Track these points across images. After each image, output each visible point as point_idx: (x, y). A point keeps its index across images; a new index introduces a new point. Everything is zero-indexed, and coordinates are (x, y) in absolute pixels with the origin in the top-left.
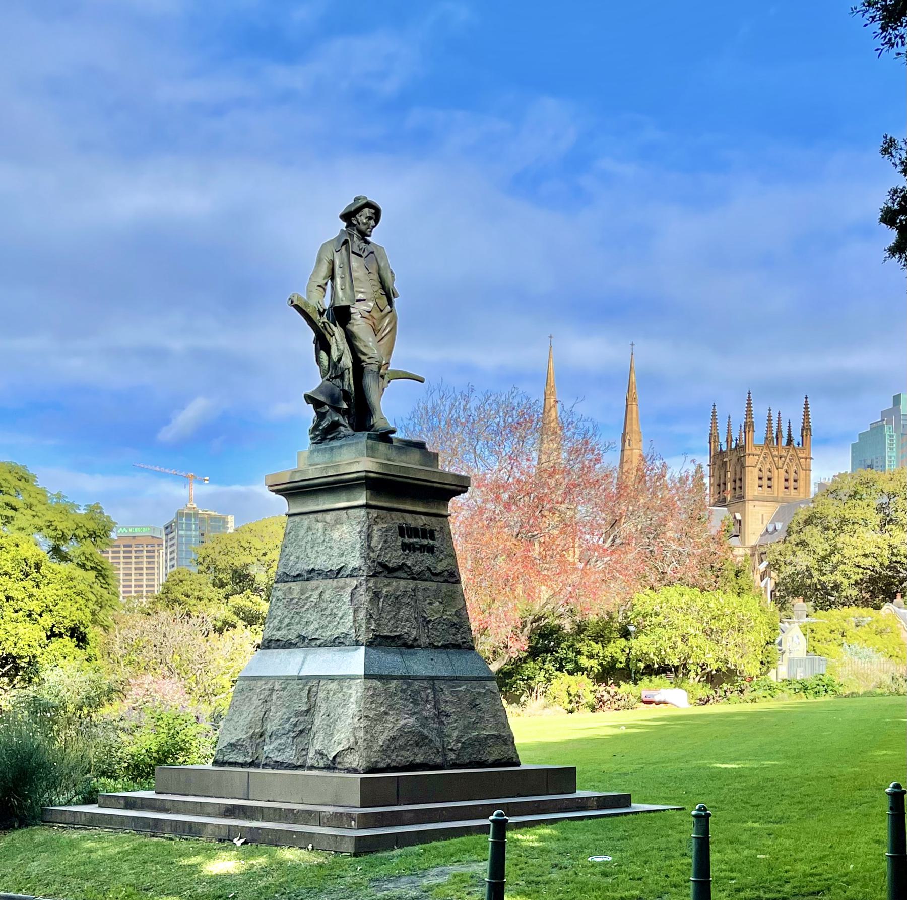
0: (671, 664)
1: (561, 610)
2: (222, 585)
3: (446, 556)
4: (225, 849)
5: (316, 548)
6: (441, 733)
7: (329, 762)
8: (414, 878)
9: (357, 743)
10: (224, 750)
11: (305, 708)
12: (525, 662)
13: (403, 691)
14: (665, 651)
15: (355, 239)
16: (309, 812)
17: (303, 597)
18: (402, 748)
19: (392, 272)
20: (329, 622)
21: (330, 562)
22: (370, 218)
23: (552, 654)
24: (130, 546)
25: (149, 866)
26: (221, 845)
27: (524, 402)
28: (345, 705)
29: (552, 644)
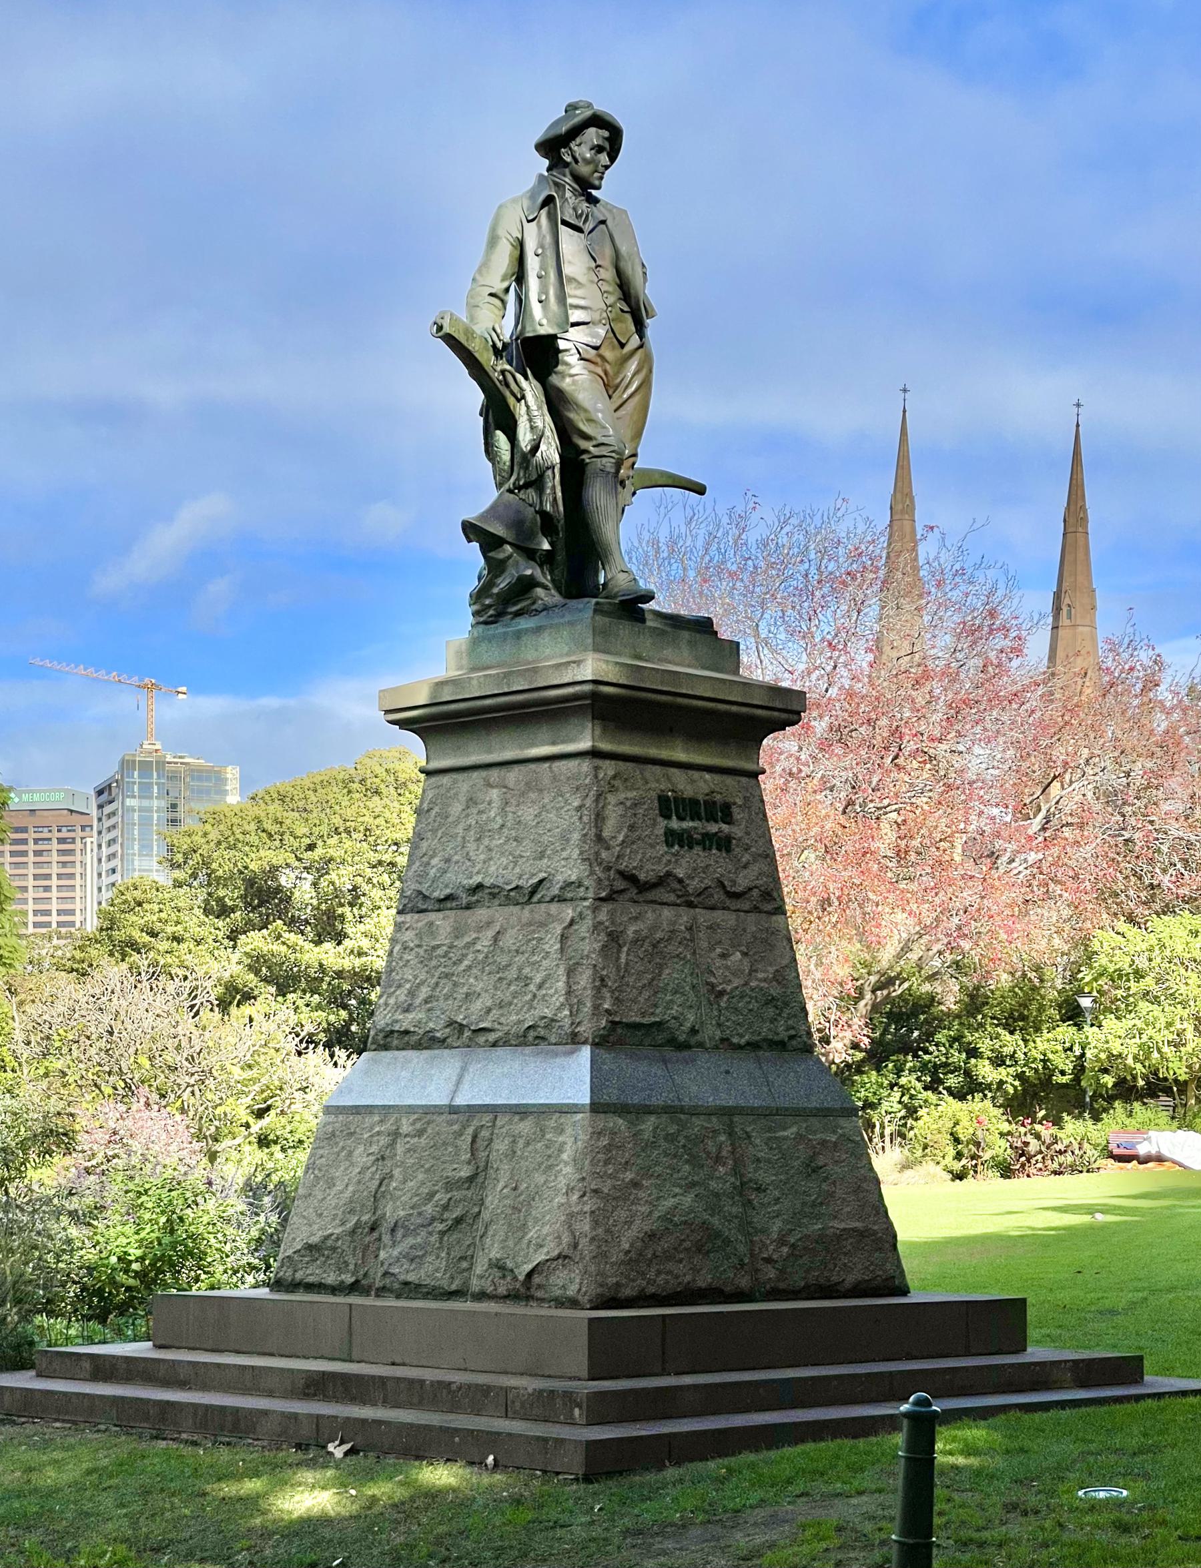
0: (1171, 1077)
1: (937, 963)
2: (224, 911)
3: (756, 857)
4: (311, 1464)
5: (486, 842)
6: (745, 1226)
7: (518, 1285)
8: (717, 1530)
9: (575, 1246)
10: (296, 1257)
11: (465, 1172)
12: (860, 1072)
13: (671, 1138)
14: (1159, 1051)
15: (568, 194)
16: (486, 1390)
17: (460, 943)
18: (668, 1256)
19: (643, 266)
20: (515, 995)
21: (517, 870)
22: (599, 149)
23: (916, 1056)
24: (24, 830)
25: (157, 1500)
26: (300, 1456)
27: (861, 528)
28: (550, 1167)
29: (916, 1033)
